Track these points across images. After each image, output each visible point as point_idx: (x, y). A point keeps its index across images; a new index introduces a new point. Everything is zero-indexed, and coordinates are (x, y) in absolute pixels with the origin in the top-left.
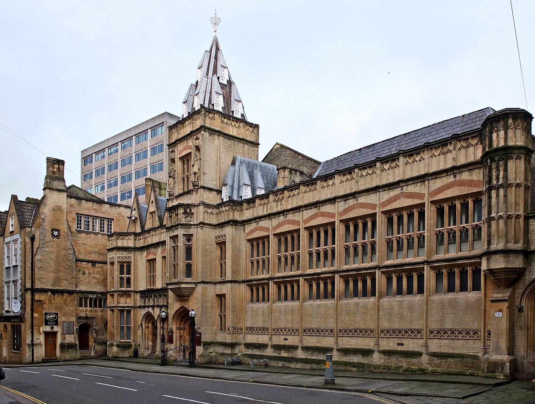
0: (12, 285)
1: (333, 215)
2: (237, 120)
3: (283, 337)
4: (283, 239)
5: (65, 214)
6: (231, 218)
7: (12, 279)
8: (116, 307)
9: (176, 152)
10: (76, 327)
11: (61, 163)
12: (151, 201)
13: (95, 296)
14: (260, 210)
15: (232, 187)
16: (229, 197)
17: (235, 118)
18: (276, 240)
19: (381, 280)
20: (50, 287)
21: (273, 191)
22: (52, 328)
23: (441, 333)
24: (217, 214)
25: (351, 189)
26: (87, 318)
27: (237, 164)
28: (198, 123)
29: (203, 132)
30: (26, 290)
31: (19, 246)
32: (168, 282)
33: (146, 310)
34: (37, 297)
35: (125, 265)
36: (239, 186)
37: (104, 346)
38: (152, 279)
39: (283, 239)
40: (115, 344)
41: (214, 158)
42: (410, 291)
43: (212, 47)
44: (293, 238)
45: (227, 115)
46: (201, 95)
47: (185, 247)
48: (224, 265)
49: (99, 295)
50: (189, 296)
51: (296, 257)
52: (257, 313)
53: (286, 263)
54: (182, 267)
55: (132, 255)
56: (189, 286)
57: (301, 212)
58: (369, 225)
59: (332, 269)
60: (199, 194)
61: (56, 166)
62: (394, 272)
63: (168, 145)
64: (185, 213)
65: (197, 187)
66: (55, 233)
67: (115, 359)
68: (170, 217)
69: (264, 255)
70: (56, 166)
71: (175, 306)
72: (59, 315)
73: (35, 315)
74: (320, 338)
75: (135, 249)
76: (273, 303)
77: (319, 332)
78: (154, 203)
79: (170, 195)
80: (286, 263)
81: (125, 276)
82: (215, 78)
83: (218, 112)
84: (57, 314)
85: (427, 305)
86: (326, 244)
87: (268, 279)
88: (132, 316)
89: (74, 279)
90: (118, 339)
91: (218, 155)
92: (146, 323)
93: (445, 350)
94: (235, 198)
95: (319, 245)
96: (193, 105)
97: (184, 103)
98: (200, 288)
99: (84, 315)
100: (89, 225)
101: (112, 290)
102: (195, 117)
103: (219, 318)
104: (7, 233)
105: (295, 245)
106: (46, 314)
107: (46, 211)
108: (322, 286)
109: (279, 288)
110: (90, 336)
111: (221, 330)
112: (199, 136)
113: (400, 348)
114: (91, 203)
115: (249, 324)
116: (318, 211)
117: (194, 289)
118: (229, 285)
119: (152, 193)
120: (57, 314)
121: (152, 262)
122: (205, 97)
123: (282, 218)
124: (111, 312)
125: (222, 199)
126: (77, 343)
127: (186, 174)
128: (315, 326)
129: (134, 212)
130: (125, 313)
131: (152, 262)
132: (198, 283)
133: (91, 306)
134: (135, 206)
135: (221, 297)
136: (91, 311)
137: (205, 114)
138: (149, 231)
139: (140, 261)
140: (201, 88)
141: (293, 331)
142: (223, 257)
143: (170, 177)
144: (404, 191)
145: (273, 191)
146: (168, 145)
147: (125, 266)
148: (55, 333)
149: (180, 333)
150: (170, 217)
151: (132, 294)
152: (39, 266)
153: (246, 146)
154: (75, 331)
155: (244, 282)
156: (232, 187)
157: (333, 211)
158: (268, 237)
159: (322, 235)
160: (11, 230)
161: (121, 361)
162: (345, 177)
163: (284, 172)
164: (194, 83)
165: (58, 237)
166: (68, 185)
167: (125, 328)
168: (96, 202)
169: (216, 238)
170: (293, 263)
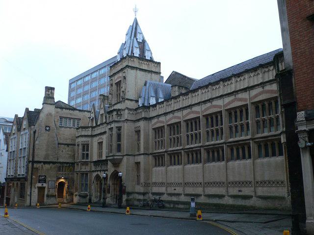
0: (22, 159)
2: (147, 60)
3: (173, 188)
7: (23, 156)
11: (53, 89)
14: (160, 110)
18: (205, 120)
19: (227, 151)
20: (42, 160)
21: (168, 98)
22: (42, 184)
23: (263, 183)
24: (135, 114)
25: (208, 97)
27: (148, 85)
28: (125, 64)
30: (30, 162)
31: (27, 136)
32: (107, 155)
33: (96, 173)
34: (35, 165)
36: (148, 98)
38: (100, 154)
41: (134, 81)
42: (244, 158)
45: (142, 58)
46: (127, 49)
50: (119, 163)
52: (158, 173)
53: (174, 142)
56: (119, 157)
58: (219, 117)
61: (50, 91)
62: (235, 145)
64: (117, 114)
65: (124, 99)
66: (48, 128)
70: (50, 91)
71: (111, 169)
73: (34, 177)
77: (194, 184)
82: (135, 39)
84: (45, 176)
85: (254, 165)
88: (89, 177)
93: (266, 194)
94: (146, 104)
98: (125, 158)
101: (78, 161)
102: (124, 61)
104: (22, 129)
105: (179, 132)
106: (39, 176)
107: (42, 116)
108: (195, 155)
109: (171, 157)
112: (125, 70)
113: (240, 194)
117: (121, 160)
118: (142, 156)
120: (45, 176)
121: (100, 144)
126: (56, 194)
132: (124, 155)
134: (93, 111)
135: (138, 164)
138: (99, 125)
141: (246, 183)
143: (110, 94)
144: (213, 104)
145: (168, 98)
148: (44, 188)
149: (114, 187)
155: (151, 154)
156: (144, 98)
160: (24, 127)
162: (205, 90)
164: (124, 43)
165: (49, 130)
166: (56, 101)
167: (84, 185)
170: (178, 142)
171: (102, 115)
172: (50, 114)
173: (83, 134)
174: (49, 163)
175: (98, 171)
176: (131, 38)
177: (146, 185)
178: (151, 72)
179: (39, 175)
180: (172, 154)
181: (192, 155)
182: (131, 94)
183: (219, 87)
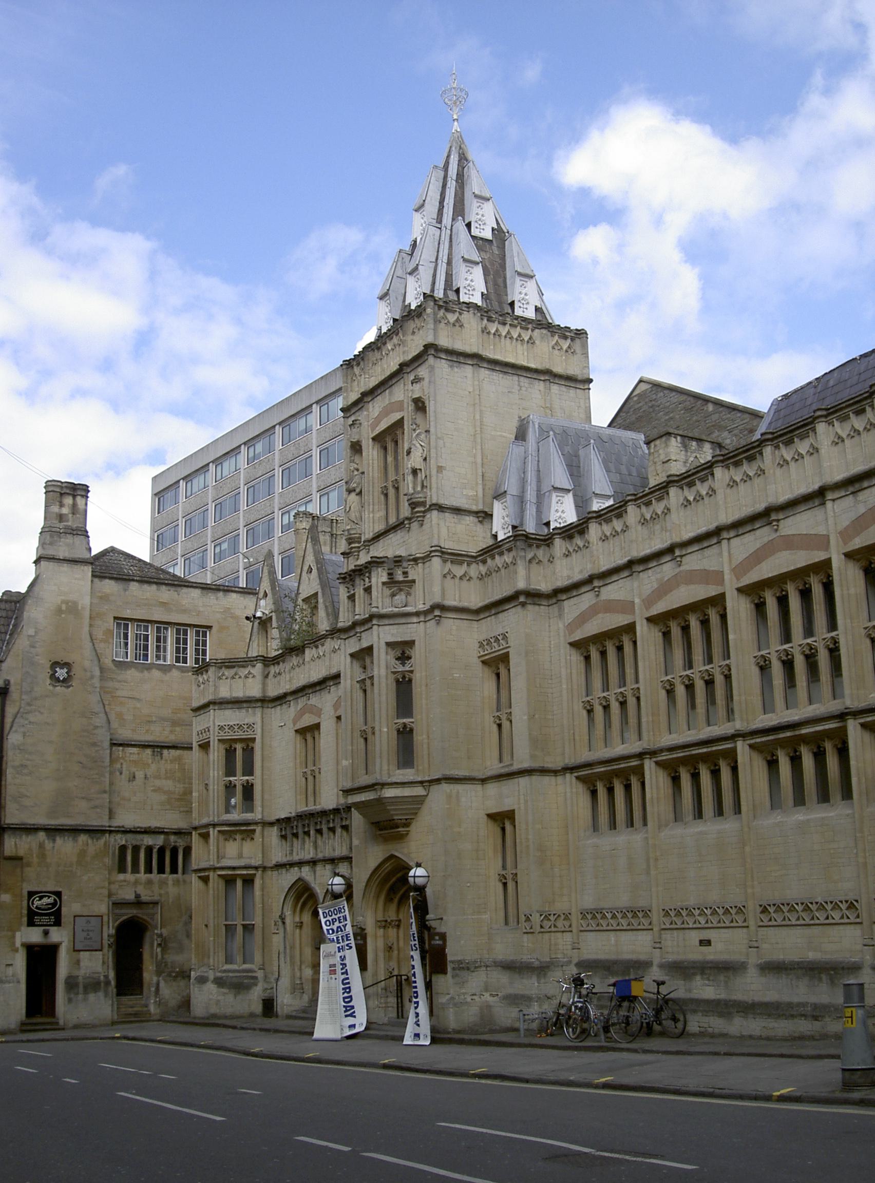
1: (823, 542)
3: (694, 937)
4: (676, 632)
5: (86, 621)
6: (521, 585)
8: (215, 869)
9: (365, 424)
10: (110, 930)
12: (306, 568)
13: (159, 841)
14: (602, 552)
15: (521, 500)
16: (514, 527)
17: (517, 318)
22: (46, 933)
24: (481, 578)
26: (138, 903)
27: (532, 436)
28: (414, 346)
29: (431, 360)
32: (348, 785)
35: (239, 747)
37: (182, 983)
39: (676, 632)
40: (212, 977)
41: (467, 429)
43: (448, 156)
44: (705, 623)
45: (497, 309)
46: (425, 273)
47: (392, 678)
48: (506, 724)
49: (172, 838)
50: (407, 825)
51: (719, 680)
54: (385, 737)
55: (258, 719)
56: (407, 792)
57: (725, 542)
58: (818, 591)
59: (834, 706)
60: (426, 526)
61: (66, 500)
63: (342, 410)
64: (391, 582)
65: (420, 509)
66: (61, 672)
67: (211, 1022)
68: (352, 598)
69: (623, 682)
70: (66, 500)
71: (371, 857)
72: (64, 897)
74: (816, 930)
75: (265, 702)
76: (660, 827)
77: (810, 912)
78: (315, 571)
79: (350, 541)
80: (692, 704)
81: (239, 779)
82: (460, 225)
83: (469, 305)
84: (58, 894)
86: (809, 631)
87: (641, 756)
89: (106, 796)
90: (217, 964)
91: (478, 417)
92: (294, 912)
94: (530, 527)
95: (787, 637)
96: (404, 301)
97: (381, 298)
99: (130, 897)
100: (146, 648)
101: (205, 821)
102: (411, 325)
103: (500, 886)
106: (31, 894)
107: (36, 616)
108: (808, 762)
110: (146, 956)
111: (506, 923)
112: (422, 371)
114: (154, 587)
115: (588, 902)
116: (774, 536)
117: (419, 801)
119: (309, 545)
120: (58, 894)
122: (434, 276)
123: (667, 569)
124: (201, 884)
125: (495, 536)
127: (392, 477)
128: (794, 892)
129: (262, 603)
130: (239, 883)
131: (308, 732)
132: (431, 782)
133: (149, 870)
135: (502, 819)
136: (150, 882)
137: (435, 314)
139: (276, 734)
140: (425, 255)
141: (730, 915)
142: (503, 702)
143: (350, 491)
145: (643, 495)
146: (342, 410)
147: (239, 753)
148: (53, 950)
149: (385, 937)
150: (352, 598)
151: (258, 829)
152: (17, 763)
153: (555, 388)
154: (106, 943)
156: (521, 500)
157: (821, 530)
158: (630, 629)
159: (795, 603)
161: (225, 1026)
163: (667, 446)
164: (408, 248)
165: (66, 681)
166: (97, 548)
167: (240, 929)
168: (167, 584)
169: (481, 645)
171: (312, 600)
172: (72, 608)
173: (225, 692)
174: (75, 831)
175: (300, 864)
176: (439, 220)
177: (547, 924)
178: (549, 375)
179: (27, 887)
180: (684, 761)
181: (796, 760)
182: (455, 483)
183: (712, 492)
